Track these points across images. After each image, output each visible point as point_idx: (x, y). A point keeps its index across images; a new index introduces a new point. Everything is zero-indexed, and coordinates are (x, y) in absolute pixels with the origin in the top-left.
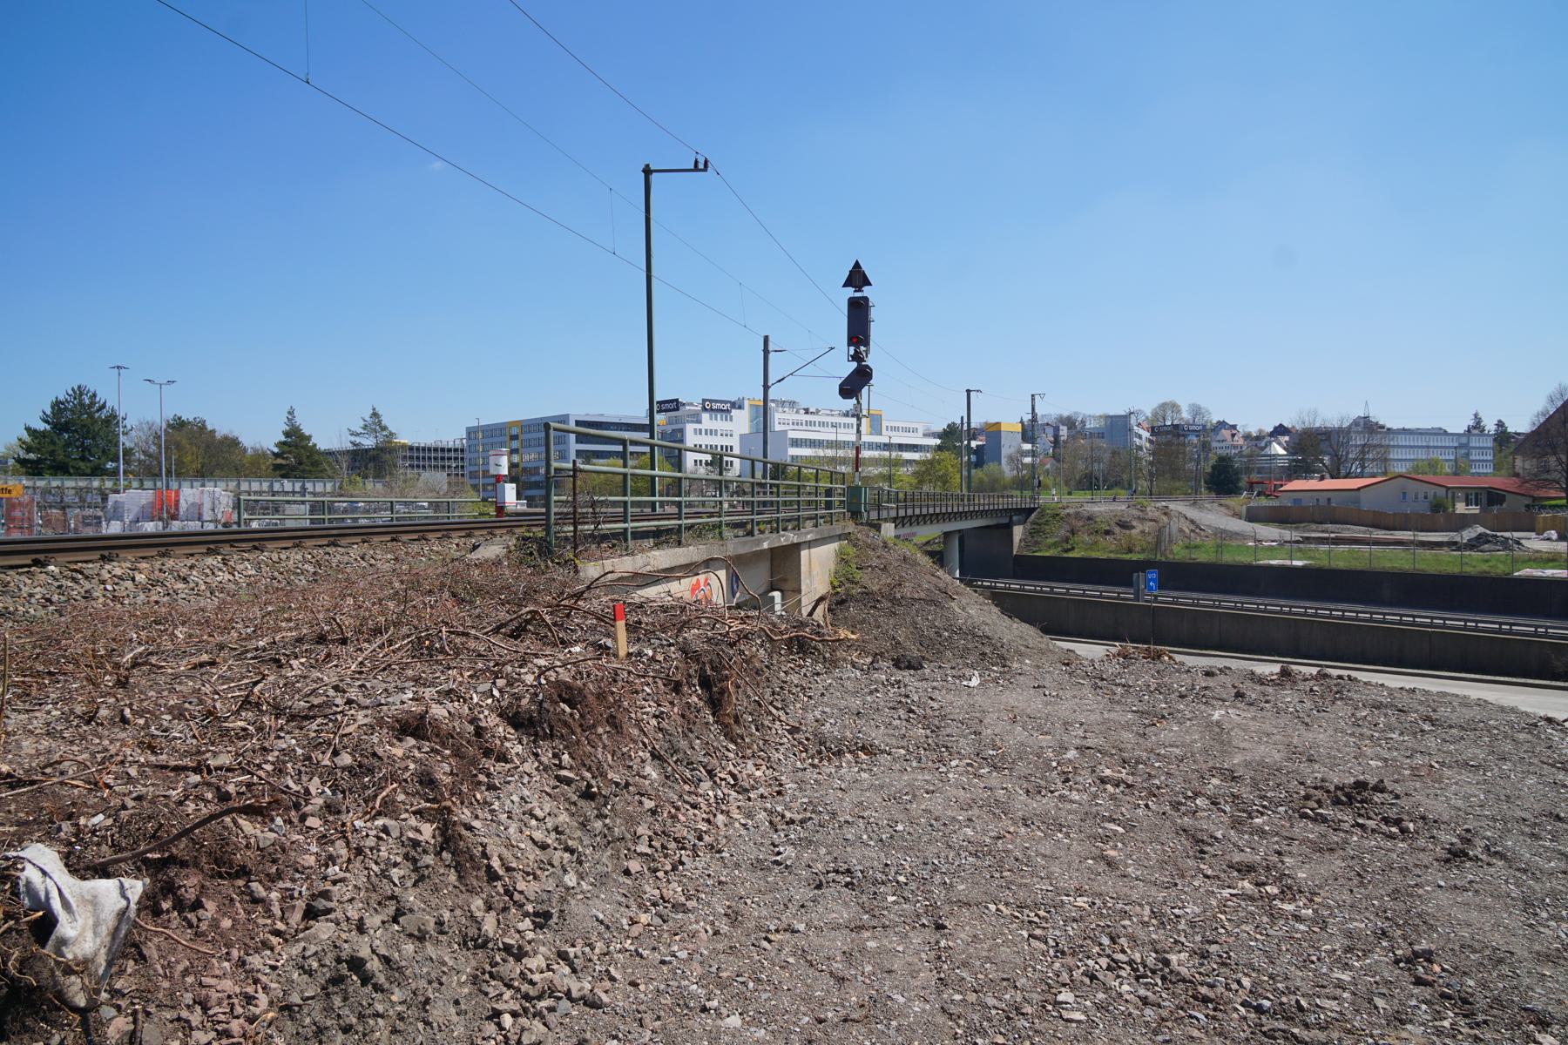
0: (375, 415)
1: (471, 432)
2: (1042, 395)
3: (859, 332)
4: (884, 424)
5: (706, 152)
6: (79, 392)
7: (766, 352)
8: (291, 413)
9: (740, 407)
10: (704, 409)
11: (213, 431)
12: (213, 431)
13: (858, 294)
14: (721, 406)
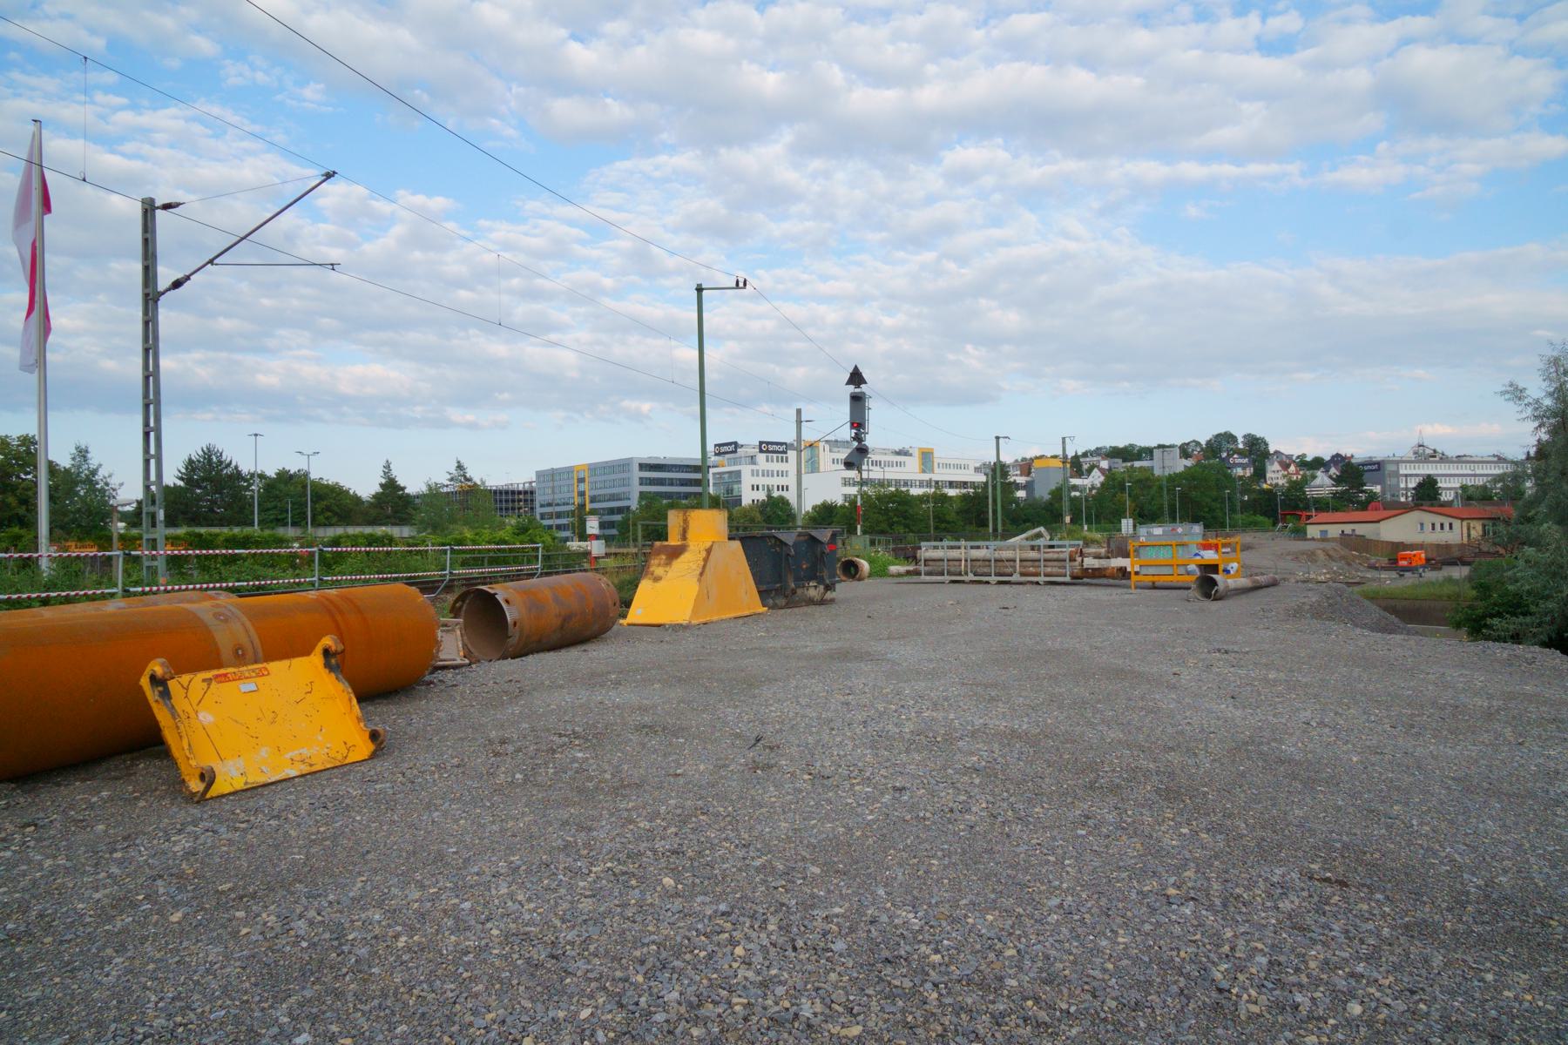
0: (460, 467)
1: (540, 474)
4: (936, 461)
5: (742, 276)
6: (208, 453)
8: (388, 466)
10: (761, 451)
11: (382, 485)
12: (382, 485)
14: (777, 448)
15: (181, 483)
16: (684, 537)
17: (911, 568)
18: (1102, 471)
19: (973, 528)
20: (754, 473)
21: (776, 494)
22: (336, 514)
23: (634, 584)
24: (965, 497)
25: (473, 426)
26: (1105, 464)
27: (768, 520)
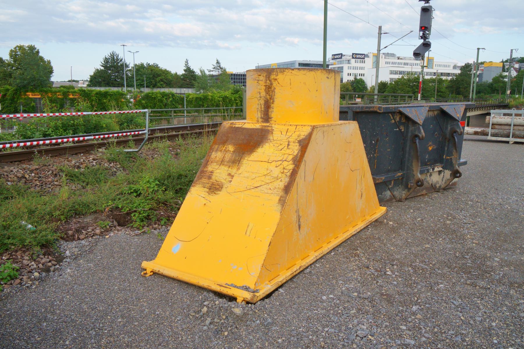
0: (218, 62)
2: (517, 50)
3: (425, 28)
6: (113, 55)
7: (380, 34)
8: (187, 62)
9: (368, 57)
10: (353, 58)
11: (185, 70)
12: (185, 70)
13: (427, 5)
14: (360, 56)
15: (103, 68)
16: (266, 118)
17: (479, 130)
18: (515, 69)
19: (454, 95)
20: (349, 68)
21: (358, 77)
22: (165, 83)
23: (182, 192)
24: (452, 81)
25: (228, 48)
26: (517, 66)
27: (354, 90)
